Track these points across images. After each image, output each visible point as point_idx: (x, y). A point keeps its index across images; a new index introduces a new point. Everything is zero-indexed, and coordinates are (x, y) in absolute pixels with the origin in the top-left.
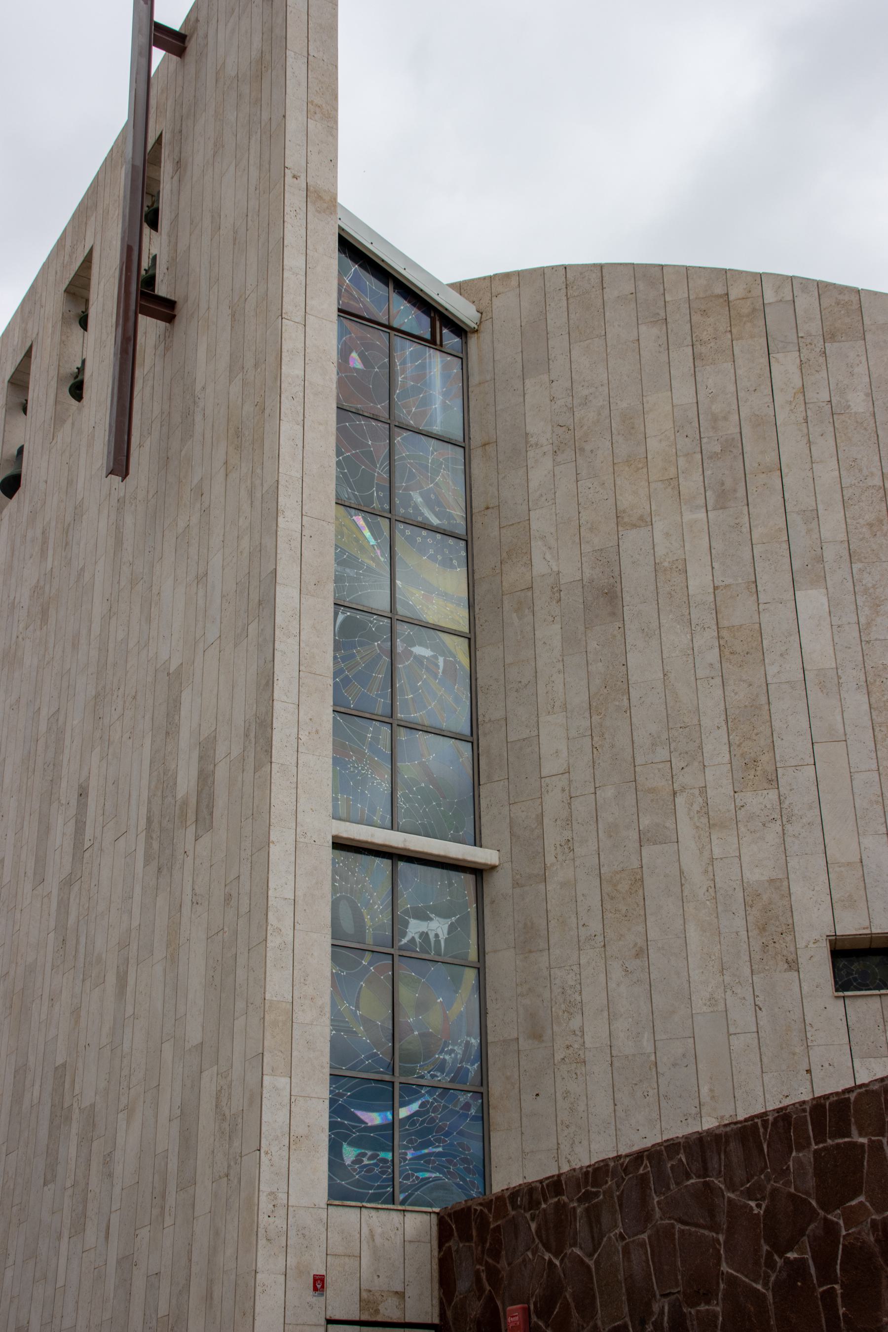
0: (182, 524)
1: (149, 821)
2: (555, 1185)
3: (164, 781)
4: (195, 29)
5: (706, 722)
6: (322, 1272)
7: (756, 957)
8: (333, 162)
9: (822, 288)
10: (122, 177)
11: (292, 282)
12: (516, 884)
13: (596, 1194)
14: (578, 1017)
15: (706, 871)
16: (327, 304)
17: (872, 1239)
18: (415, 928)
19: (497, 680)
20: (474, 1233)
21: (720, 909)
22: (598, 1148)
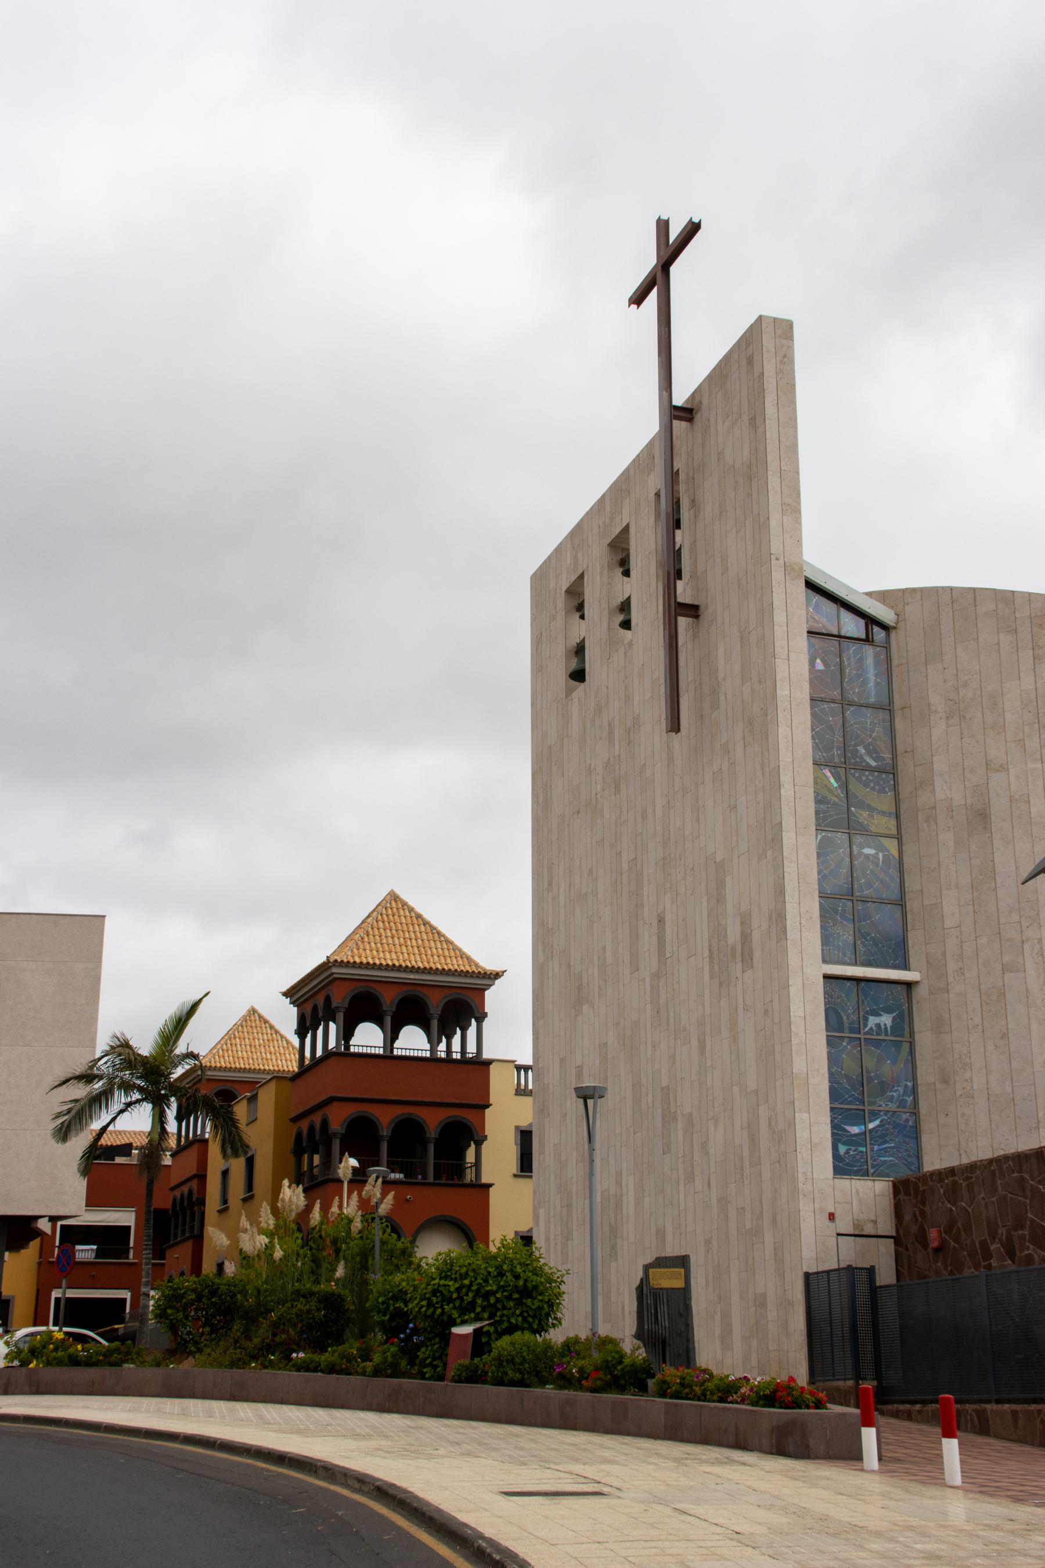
2: (952, 1171)
3: (718, 931)
8: (799, 541)
11: (779, 631)
12: (931, 993)
18: (873, 1021)
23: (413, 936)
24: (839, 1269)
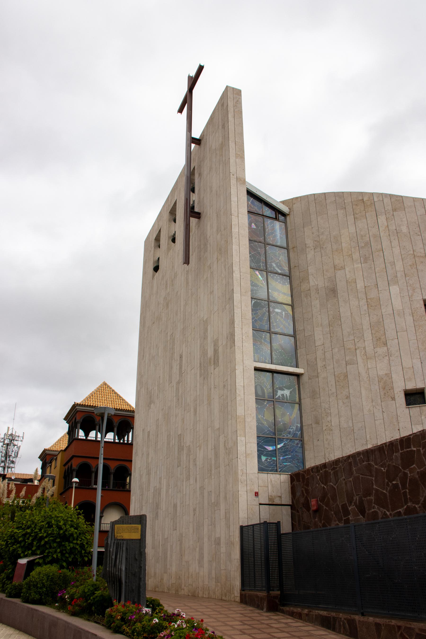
0: (205, 277)
1: (200, 364)
2: (324, 466)
3: (204, 353)
4: (203, 138)
5: (364, 327)
6: (257, 491)
7: (382, 397)
8: (244, 170)
9: (391, 196)
10: (184, 179)
11: (234, 204)
12: (310, 379)
13: (337, 468)
14: (330, 417)
15: (366, 372)
16: (244, 210)
17: (417, 476)
18: (280, 393)
19: (301, 318)
20: (301, 479)
21: (371, 383)
22: (337, 455)
23: (110, 397)
24: (260, 524)
